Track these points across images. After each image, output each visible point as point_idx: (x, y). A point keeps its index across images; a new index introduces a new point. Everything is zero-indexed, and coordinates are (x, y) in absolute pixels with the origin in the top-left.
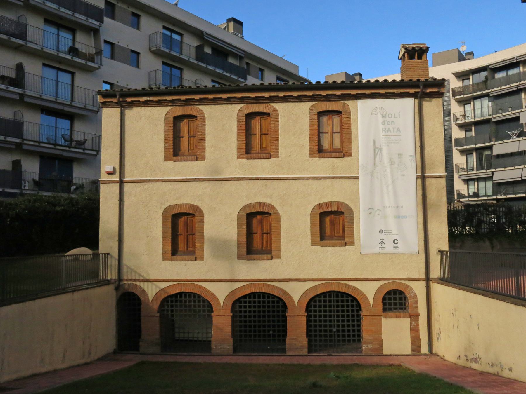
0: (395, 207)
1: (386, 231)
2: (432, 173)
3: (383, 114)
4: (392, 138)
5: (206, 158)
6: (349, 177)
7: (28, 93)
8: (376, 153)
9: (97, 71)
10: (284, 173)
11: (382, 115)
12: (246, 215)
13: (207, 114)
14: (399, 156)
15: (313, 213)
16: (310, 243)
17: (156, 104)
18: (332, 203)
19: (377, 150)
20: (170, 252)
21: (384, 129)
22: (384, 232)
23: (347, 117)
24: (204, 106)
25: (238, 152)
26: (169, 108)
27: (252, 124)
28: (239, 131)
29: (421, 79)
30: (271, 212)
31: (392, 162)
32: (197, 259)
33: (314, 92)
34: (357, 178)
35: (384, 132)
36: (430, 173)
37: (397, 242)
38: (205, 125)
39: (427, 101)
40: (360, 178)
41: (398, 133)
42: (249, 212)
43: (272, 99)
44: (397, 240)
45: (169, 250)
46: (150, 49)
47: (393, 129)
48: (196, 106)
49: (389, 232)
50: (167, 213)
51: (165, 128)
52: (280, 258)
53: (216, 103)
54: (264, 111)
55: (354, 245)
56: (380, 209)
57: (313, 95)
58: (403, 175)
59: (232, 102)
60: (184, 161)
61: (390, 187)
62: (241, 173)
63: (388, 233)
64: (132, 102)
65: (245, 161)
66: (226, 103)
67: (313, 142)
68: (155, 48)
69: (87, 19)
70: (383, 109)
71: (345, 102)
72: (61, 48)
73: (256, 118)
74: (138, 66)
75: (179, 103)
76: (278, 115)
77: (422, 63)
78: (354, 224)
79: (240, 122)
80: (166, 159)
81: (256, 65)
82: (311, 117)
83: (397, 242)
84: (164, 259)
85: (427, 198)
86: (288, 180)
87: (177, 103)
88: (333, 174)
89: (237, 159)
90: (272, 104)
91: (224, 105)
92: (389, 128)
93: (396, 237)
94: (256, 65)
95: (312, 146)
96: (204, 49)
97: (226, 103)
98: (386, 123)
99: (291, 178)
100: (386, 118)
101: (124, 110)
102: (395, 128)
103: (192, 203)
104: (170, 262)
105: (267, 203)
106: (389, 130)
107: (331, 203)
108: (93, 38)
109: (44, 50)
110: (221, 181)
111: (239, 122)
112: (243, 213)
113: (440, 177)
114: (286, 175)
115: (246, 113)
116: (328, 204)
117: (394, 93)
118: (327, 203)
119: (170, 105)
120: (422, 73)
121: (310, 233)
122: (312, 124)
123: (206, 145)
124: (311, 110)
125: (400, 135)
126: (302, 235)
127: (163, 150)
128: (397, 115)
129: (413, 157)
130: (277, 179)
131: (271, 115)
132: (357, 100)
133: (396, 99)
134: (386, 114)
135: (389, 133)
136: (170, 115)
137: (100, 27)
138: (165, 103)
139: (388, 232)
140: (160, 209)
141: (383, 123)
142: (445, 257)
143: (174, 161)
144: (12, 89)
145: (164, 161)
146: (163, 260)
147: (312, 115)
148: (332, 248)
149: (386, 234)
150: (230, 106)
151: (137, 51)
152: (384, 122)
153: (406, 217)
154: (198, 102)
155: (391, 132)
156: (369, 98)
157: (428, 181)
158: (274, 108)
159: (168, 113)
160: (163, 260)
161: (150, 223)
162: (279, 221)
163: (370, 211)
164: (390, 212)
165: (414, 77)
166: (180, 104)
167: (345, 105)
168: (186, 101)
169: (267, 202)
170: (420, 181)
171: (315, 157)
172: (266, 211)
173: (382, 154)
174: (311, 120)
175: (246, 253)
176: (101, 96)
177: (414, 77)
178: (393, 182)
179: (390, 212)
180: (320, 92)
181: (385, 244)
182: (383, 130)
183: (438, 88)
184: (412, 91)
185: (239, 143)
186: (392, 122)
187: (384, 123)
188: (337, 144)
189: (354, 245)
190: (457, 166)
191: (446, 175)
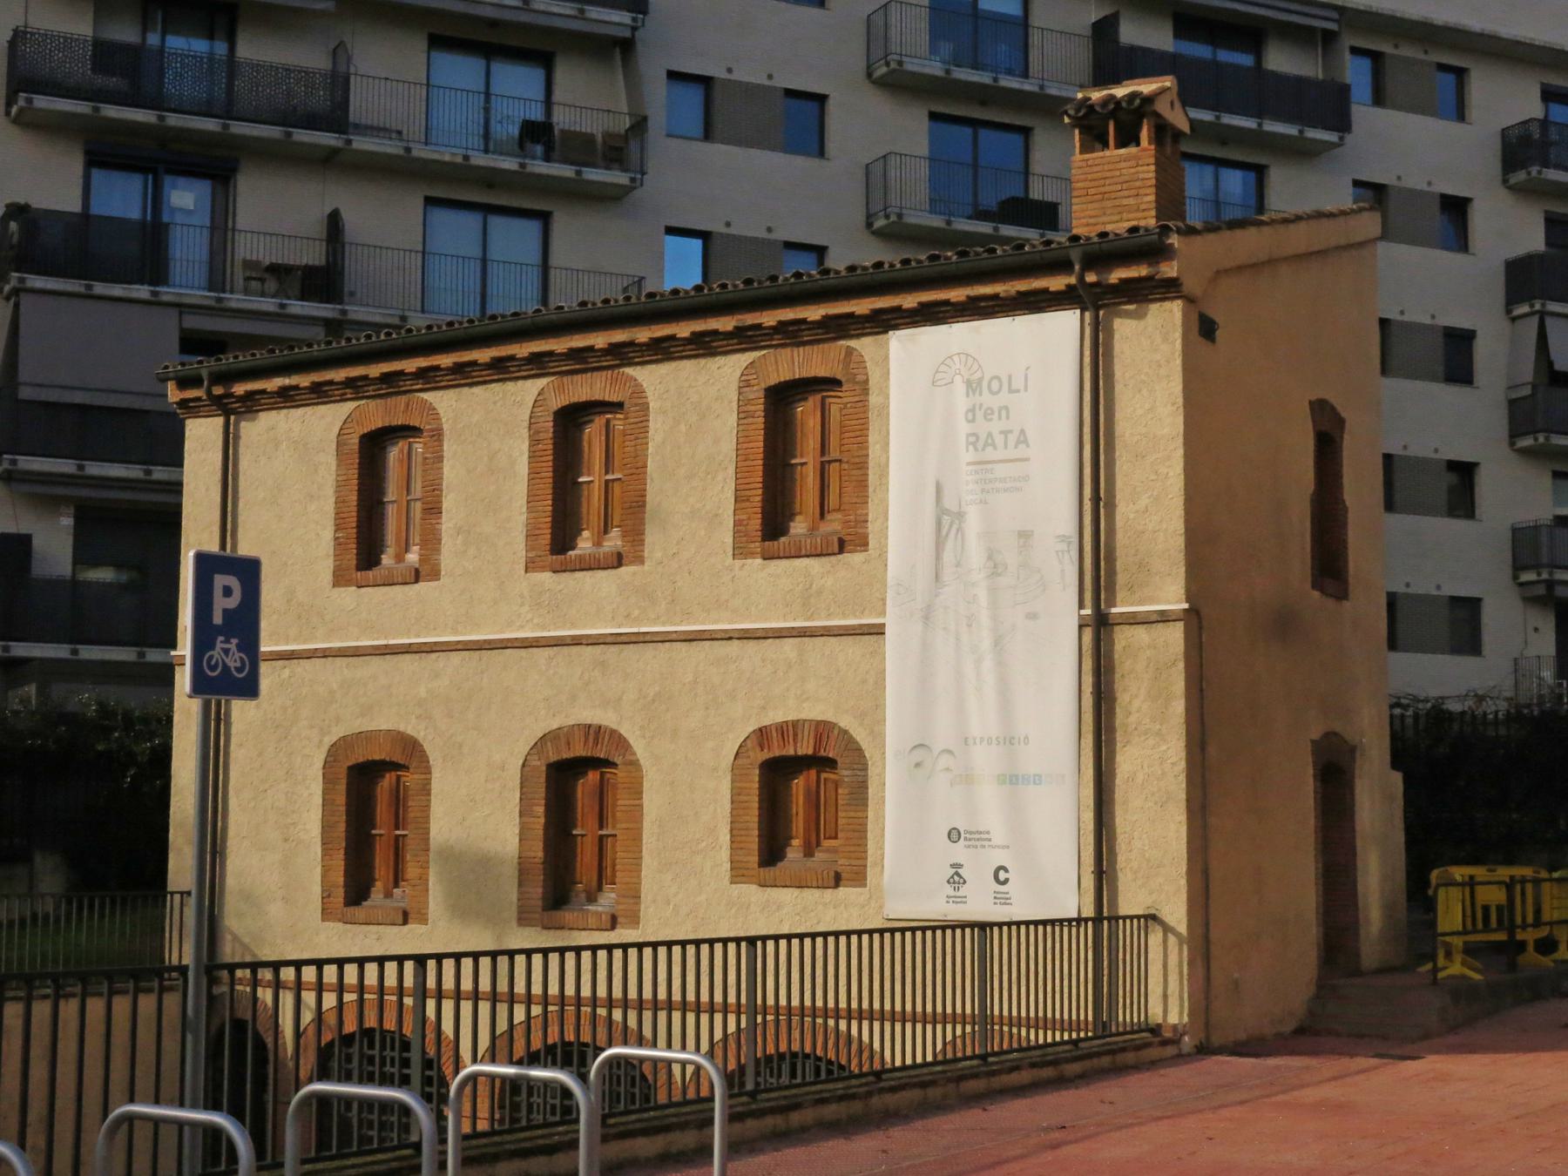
0: (1001, 740)
1: (971, 833)
2: (1141, 603)
3: (972, 378)
4: (1001, 471)
5: (443, 573)
6: (853, 627)
7: (357, 312)
8: (944, 533)
9: (637, 193)
10: (655, 621)
11: (968, 383)
12: (544, 768)
13: (448, 420)
14: (1022, 541)
15: (740, 761)
16: (728, 874)
17: (312, 396)
18: (800, 727)
19: (946, 521)
20: (340, 893)
21: (972, 439)
22: (963, 836)
23: (857, 399)
24: (440, 393)
25: (529, 549)
26: (349, 406)
27: (586, 437)
28: (533, 474)
29: (1109, 228)
30: (618, 760)
31: (995, 566)
32: (410, 920)
33: (740, 317)
34: (878, 631)
35: (971, 448)
36: (1132, 605)
37: (1007, 875)
38: (440, 459)
39: (1128, 315)
40: (888, 630)
41: (1021, 451)
42: (554, 758)
43: (622, 355)
44: (1006, 871)
45: (338, 887)
46: (869, 75)
47: (1003, 436)
48: (419, 394)
49: (978, 838)
50: (334, 761)
51: (338, 475)
52: (638, 923)
53: (433, 385)
54: (607, 399)
55: (865, 885)
56: (951, 748)
57: (736, 328)
58: (1032, 616)
59: (513, 372)
60: (384, 585)
61: (988, 664)
62: (535, 621)
63: (978, 840)
64: (250, 395)
65: (546, 577)
66: (496, 377)
67: (748, 500)
68: (884, 70)
69: (582, 11)
70: (970, 360)
71: (853, 343)
72: (499, 131)
73: (591, 421)
74: (821, 153)
75: (371, 388)
76: (645, 408)
77: (1133, 163)
78: (866, 805)
79: (538, 441)
80: (340, 580)
81: (1421, 56)
82: (745, 409)
83: (1007, 875)
84: (327, 914)
85: (1118, 701)
86: (667, 644)
87: (366, 388)
88: (808, 619)
89: (526, 572)
90: (629, 371)
91: (493, 385)
92: (990, 435)
93: (1000, 858)
94: (1421, 56)
95: (744, 517)
96: (1116, 32)
97: (496, 377)
98: (979, 414)
99: (674, 636)
100: (981, 394)
101: (237, 424)
102: (1011, 432)
103: (402, 729)
104: (340, 925)
105: (606, 728)
106: (990, 442)
107: (795, 724)
108: (620, 71)
109: (415, 153)
110: (478, 652)
111: (534, 442)
112: (539, 763)
113: (1164, 618)
114: (664, 624)
115: (555, 408)
116: (788, 730)
117: (995, 297)
118: (785, 725)
119: (349, 396)
120: (1131, 201)
121: (728, 837)
122: (746, 433)
123: (444, 527)
124: (745, 384)
125: (1027, 460)
126: (704, 844)
127: (331, 552)
128: (1018, 383)
129: (1069, 543)
130: (634, 639)
131: (626, 406)
132: (886, 332)
133: (1018, 318)
134: (980, 380)
135: (990, 454)
136: (352, 431)
137: (634, 29)
138: (336, 392)
139: (977, 836)
140: (319, 747)
141: (970, 416)
142: (1172, 939)
143: (359, 587)
144: (297, 307)
145: (334, 586)
146: (323, 920)
147: (749, 402)
148: (796, 892)
149: (969, 847)
150: (510, 386)
151: (809, 90)
152: (972, 410)
153: (1037, 779)
154: (421, 381)
155: (995, 448)
156: (926, 321)
157: (1123, 638)
158: (636, 385)
159: (346, 426)
160: (323, 920)
161: (293, 793)
162: (638, 793)
163: (919, 755)
164: (985, 760)
165: (1101, 220)
166: (374, 391)
167: (851, 354)
168: (386, 378)
169: (604, 723)
170: (1088, 634)
171: (752, 555)
172: (602, 756)
173: (963, 535)
174: (745, 421)
175: (540, 903)
176: (174, 382)
177: (1101, 220)
178: (998, 642)
179: (985, 760)
180: (758, 314)
181: (965, 882)
182: (968, 443)
183: (1150, 265)
184: (1057, 283)
185: (534, 514)
186: (1000, 410)
187: (974, 415)
188: (220, 581)
189: (865, 885)
190: (236, 668)
191: (1185, 610)
